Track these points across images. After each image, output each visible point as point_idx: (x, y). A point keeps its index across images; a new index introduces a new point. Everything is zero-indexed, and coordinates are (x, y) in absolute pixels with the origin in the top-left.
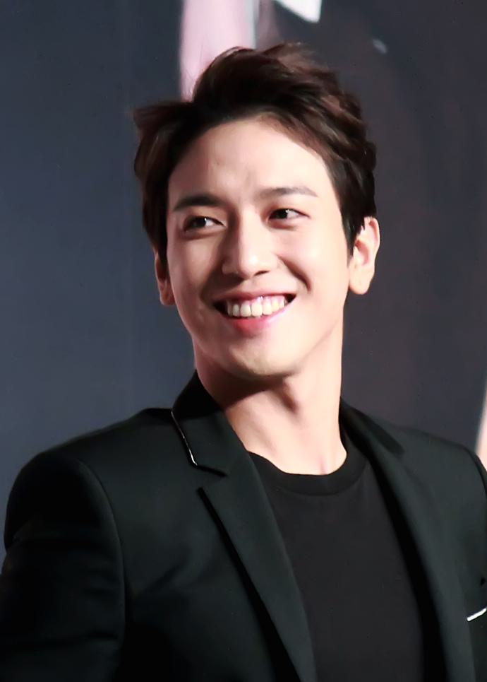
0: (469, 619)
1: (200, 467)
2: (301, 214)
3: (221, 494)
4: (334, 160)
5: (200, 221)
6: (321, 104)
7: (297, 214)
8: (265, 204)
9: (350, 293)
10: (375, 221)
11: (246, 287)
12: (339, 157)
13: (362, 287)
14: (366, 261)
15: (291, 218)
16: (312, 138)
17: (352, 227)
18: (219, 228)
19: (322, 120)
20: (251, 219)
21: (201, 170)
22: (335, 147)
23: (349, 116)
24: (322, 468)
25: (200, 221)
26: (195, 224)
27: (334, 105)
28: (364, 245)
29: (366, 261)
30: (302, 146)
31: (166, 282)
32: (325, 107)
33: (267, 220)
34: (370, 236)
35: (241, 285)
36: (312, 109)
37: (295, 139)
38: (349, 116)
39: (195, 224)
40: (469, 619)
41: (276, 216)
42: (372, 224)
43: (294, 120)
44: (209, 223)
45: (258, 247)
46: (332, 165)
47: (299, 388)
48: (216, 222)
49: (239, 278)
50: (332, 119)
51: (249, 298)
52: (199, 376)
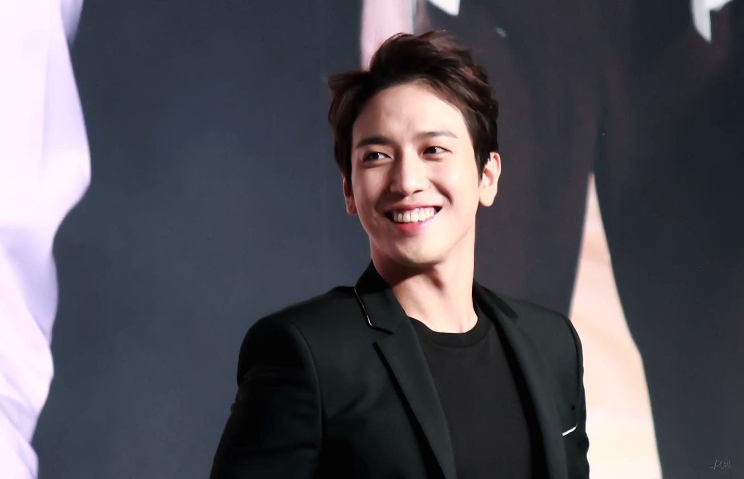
0: (564, 434)
2: (446, 150)
3: (389, 346)
5: (375, 155)
6: (460, 73)
7: (443, 150)
8: (420, 143)
9: (480, 205)
10: (498, 155)
11: (407, 201)
12: (472, 110)
13: (488, 201)
14: (491, 183)
15: (439, 153)
16: (453, 97)
17: (482, 160)
18: (388, 160)
19: (461, 84)
20: (410, 154)
21: (375, 119)
22: (470, 103)
23: (480, 81)
25: (375, 155)
26: (371, 157)
27: (469, 74)
28: (490, 172)
30: (446, 103)
31: (351, 198)
32: (463, 75)
33: (422, 154)
34: (494, 165)
36: (454, 76)
38: (480, 81)
39: (371, 157)
40: (564, 434)
41: (428, 152)
42: (495, 157)
43: (441, 84)
44: (381, 157)
45: (416, 174)
46: (467, 116)
47: (444, 272)
48: (386, 156)
49: (402, 195)
51: (409, 209)
52: (374, 264)
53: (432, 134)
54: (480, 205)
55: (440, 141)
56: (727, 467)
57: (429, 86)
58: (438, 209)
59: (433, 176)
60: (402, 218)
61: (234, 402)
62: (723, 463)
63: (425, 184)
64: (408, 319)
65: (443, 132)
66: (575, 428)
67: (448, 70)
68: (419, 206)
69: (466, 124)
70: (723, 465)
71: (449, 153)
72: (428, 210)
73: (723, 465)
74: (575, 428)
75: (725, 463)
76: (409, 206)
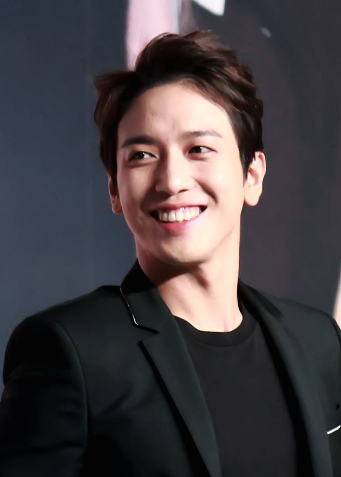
1: (140, 327)
2: (211, 150)
3: (155, 345)
4: (234, 112)
5: (140, 155)
6: (225, 73)
7: (208, 150)
8: (185, 143)
9: (245, 205)
10: (263, 154)
11: (172, 201)
12: (237, 110)
13: (253, 201)
14: (256, 182)
15: (204, 153)
16: (218, 96)
17: (247, 159)
18: (153, 159)
19: (226, 84)
20: (176, 153)
21: (141, 119)
22: (235, 103)
23: (245, 81)
24: (226, 327)
25: (140, 155)
26: (137, 157)
27: (234, 74)
28: (255, 171)
29: (256, 182)
30: (211, 102)
31: (116, 197)
32: (228, 75)
33: (187, 154)
34: (259, 165)
35: (169, 199)
36: (219, 76)
37: (207, 97)
38: (245, 81)
39: (137, 157)
41: (193, 151)
42: (260, 157)
43: (206, 84)
44: (146, 156)
45: (181, 173)
46: (232, 116)
47: (210, 271)
48: (152, 155)
49: (167, 194)
50: (232, 83)
51: (174, 208)
52: (140, 263)
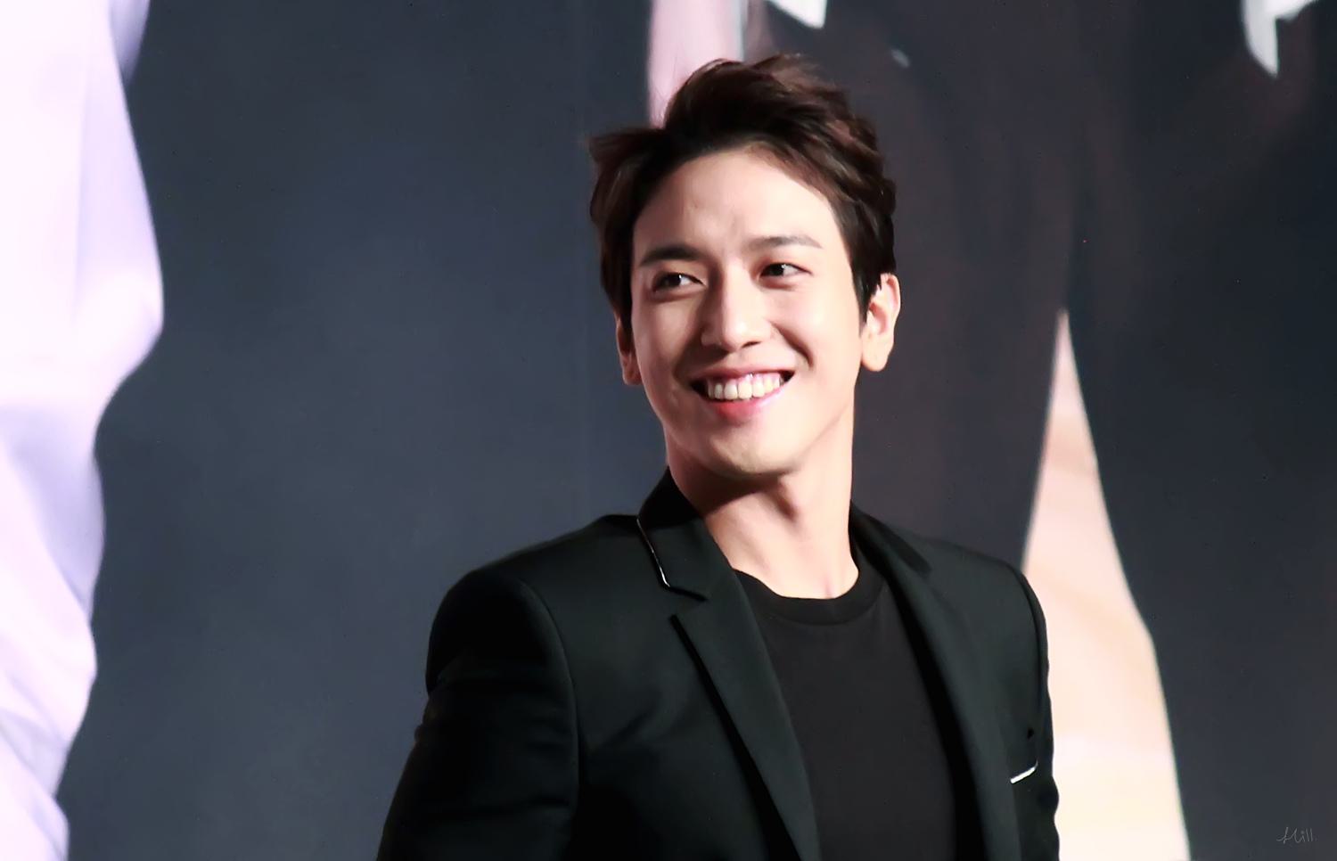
0: (1014, 781)
2: (801, 270)
3: (699, 623)
5: (674, 279)
6: (827, 131)
7: (796, 270)
8: (755, 257)
9: (863, 369)
10: (895, 279)
11: (732, 362)
12: (848, 198)
13: (878, 362)
14: (883, 329)
15: (788, 275)
16: (814, 174)
17: (865, 287)
18: (697, 287)
19: (828, 151)
20: (738, 276)
21: (675, 214)
22: (844, 185)
23: (862, 146)
25: (674, 279)
26: (667, 282)
27: (843, 133)
28: (880, 309)
30: (802, 185)
31: (630, 356)
32: (832, 134)
33: (758, 277)
34: (887, 297)
36: (815, 137)
38: (862, 146)
39: (667, 282)
40: (1014, 781)
41: (769, 272)
42: (890, 282)
43: (792, 151)
44: (685, 281)
45: (747, 312)
46: (840, 208)
47: (799, 489)
48: (694, 280)
49: (723, 350)
51: (735, 375)
52: (673, 475)
53: (777, 241)
54: (863, 369)
55: (791, 253)
56: (1306, 840)
57: (771, 154)
58: (786, 375)
59: (778, 316)
60: (723, 392)
61: (421, 722)
62: (1298, 833)
63: (763, 331)
64: (734, 573)
65: (796, 238)
66: (1033, 770)
67: (805, 125)
68: (753, 370)
69: (837, 223)
70: (1299, 835)
71: (807, 275)
72: (768, 378)
73: (1299, 835)
74: (1033, 770)
75: (1302, 832)
76: (735, 370)
